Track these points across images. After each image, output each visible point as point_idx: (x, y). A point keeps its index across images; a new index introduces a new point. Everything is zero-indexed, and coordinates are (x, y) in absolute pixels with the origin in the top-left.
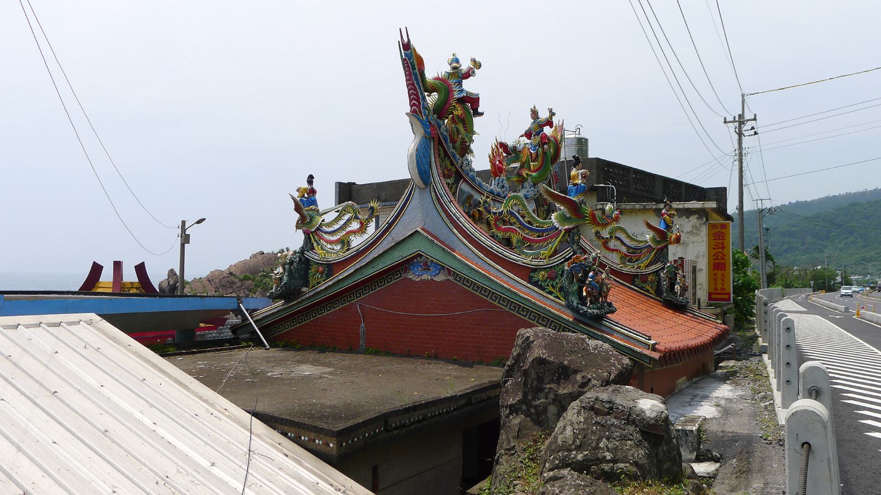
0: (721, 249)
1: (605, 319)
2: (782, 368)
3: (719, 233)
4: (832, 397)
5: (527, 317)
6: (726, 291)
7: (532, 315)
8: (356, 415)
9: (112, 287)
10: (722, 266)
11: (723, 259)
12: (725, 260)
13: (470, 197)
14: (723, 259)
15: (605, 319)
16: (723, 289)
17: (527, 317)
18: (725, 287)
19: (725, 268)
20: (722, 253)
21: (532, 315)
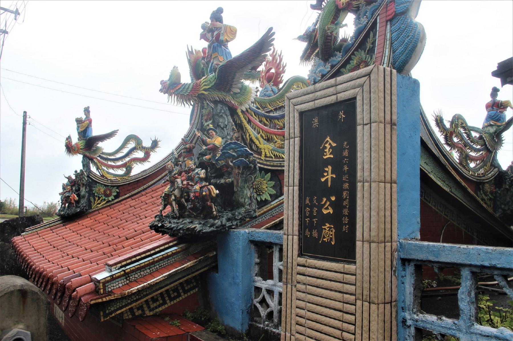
1: (59, 222)
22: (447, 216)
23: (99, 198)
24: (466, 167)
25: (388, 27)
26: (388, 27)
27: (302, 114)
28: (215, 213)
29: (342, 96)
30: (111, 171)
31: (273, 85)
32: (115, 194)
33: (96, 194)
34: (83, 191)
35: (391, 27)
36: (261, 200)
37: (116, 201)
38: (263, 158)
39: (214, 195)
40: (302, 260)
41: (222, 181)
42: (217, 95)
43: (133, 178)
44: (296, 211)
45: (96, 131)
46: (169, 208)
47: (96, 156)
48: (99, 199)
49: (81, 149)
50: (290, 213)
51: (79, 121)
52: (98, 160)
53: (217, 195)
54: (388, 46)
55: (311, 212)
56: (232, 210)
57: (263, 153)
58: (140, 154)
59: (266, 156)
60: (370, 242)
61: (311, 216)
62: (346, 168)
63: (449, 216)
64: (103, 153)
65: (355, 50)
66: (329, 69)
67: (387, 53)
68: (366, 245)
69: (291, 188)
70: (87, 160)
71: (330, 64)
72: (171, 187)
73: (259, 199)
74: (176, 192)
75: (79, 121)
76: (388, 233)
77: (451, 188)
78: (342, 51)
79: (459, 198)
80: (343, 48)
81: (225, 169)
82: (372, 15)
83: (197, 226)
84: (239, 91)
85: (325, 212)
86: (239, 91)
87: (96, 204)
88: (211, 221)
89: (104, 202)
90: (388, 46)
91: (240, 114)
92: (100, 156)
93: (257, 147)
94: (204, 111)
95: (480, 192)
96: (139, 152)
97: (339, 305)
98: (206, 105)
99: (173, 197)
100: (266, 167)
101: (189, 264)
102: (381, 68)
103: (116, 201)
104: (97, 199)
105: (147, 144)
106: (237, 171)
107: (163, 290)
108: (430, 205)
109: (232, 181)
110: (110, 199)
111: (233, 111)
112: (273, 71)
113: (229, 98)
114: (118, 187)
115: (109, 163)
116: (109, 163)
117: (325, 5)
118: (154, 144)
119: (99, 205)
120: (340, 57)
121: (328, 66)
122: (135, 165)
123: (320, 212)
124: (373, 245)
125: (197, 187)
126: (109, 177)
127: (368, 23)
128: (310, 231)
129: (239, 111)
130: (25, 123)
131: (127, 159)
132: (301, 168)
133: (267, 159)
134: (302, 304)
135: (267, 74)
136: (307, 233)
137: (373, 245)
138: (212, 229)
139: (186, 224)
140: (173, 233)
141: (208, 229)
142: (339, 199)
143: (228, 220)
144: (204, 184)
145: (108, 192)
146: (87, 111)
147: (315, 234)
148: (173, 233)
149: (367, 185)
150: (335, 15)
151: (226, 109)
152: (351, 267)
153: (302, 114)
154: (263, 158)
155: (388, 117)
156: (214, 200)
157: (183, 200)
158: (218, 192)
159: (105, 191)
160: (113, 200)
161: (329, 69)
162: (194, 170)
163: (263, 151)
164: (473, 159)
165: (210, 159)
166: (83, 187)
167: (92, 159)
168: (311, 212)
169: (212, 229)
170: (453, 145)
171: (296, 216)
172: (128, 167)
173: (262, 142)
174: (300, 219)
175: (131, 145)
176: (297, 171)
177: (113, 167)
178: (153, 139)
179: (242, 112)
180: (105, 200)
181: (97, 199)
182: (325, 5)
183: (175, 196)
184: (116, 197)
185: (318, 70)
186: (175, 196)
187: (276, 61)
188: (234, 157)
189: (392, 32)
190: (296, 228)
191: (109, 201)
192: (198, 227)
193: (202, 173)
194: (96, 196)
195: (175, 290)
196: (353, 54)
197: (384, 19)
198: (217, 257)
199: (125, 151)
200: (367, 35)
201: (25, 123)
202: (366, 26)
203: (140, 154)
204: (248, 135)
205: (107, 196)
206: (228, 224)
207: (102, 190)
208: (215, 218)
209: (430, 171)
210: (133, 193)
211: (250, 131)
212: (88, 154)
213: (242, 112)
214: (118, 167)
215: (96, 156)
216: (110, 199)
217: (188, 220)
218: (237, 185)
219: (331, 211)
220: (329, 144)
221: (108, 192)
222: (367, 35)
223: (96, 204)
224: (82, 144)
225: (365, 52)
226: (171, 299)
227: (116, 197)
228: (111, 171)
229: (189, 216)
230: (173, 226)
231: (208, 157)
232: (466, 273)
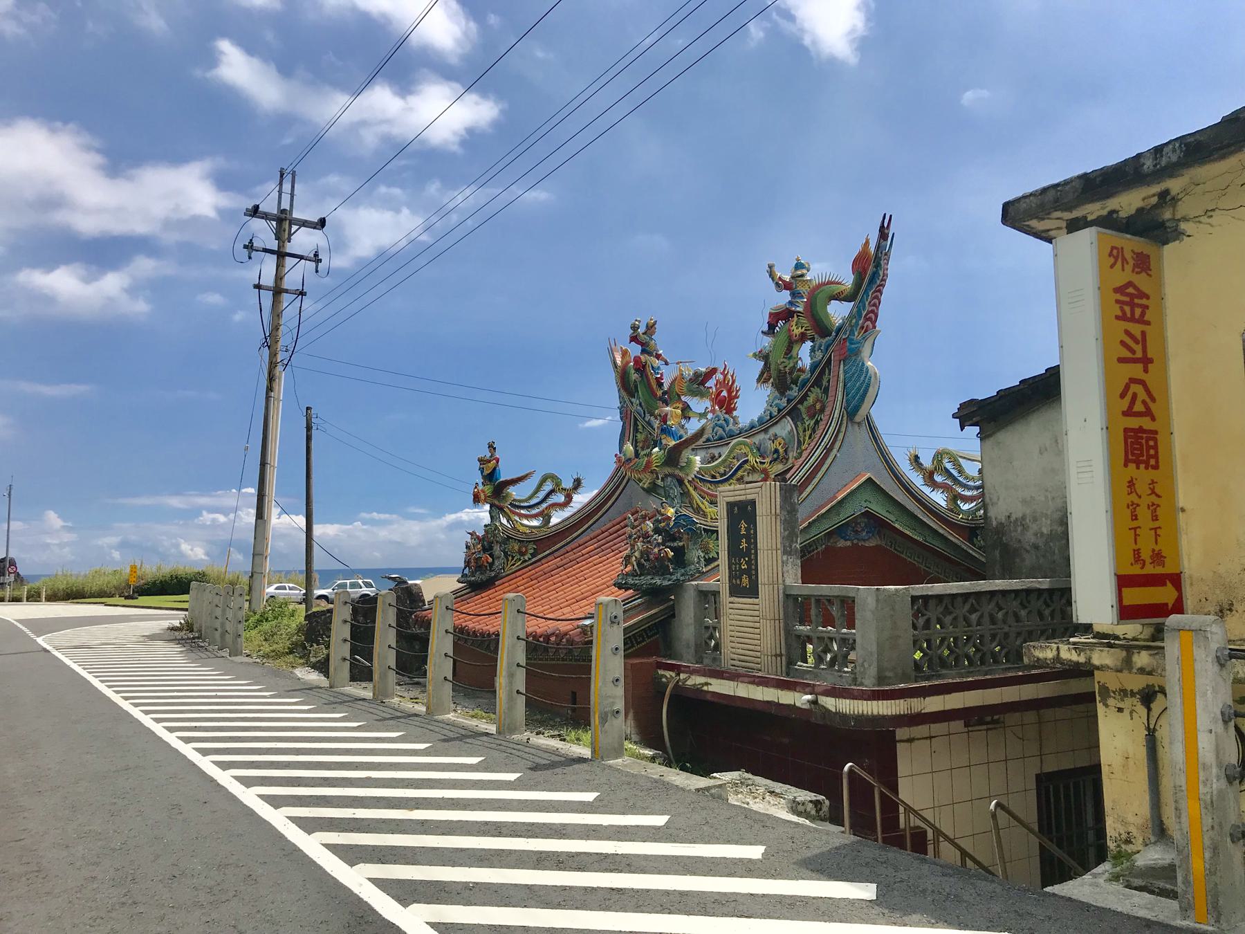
0: (1140, 366)
1: (467, 591)
2: (1053, 819)
3: (1131, 290)
4: (822, 820)
5: (636, 645)
6: (1168, 569)
7: (638, 638)
8: (310, 684)
9: (898, 745)
10: (1149, 448)
11: (1148, 413)
12: (1153, 419)
13: (765, 379)
14: (1148, 413)
15: (467, 591)
16: (1158, 557)
17: (636, 645)
18: (1162, 546)
19: (1156, 457)
20: (1142, 382)
21: (638, 638)
22: (930, 568)
23: (513, 557)
24: (957, 510)
25: (842, 366)
26: (842, 366)
27: (728, 503)
28: (671, 570)
29: (750, 497)
30: (525, 522)
31: (726, 413)
32: (532, 551)
33: (509, 553)
34: (497, 550)
35: (844, 367)
36: (709, 558)
37: (534, 560)
38: (709, 520)
39: (670, 557)
40: (732, 599)
41: (676, 544)
42: (667, 470)
43: (553, 529)
44: (727, 567)
45: (504, 476)
46: (629, 568)
47: (506, 505)
48: (512, 560)
49: (489, 497)
50: (724, 569)
51: (482, 461)
52: (508, 508)
53: (673, 556)
54: (840, 390)
55: (736, 568)
56: (684, 568)
57: (709, 516)
58: (560, 498)
59: (711, 519)
60: (765, 584)
61: (736, 571)
62: (752, 541)
63: (932, 567)
64: (514, 500)
65: (810, 387)
66: (786, 404)
67: (840, 398)
68: (763, 586)
69: (723, 552)
70: (496, 510)
71: (786, 399)
72: (631, 549)
73: (707, 557)
74: (637, 554)
75: (482, 461)
76: (775, 579)
77: (925, 537)
78: (798, 384)
79: (938, 547)
80: (799, 382)
81: (678, 535)
82: (827, 350)
83: (658, 581)
84: (685, 464)
85: (743, 567)
86: (685, 464)
87: (509, 566)
88: (669, 576)
89: (519, 563)
90: (840, 390)
91: (687, 484)
92: (511, 504)
93: (704, 511)
94: (639, 435)
95: (977, 538)
96: (558, 494)
97: (751, 624)
98: (640, 427)
99: (634, 558)
100: (711, 528)
101: (653, 612)
102: (768, 483)
103: (534, 560)
104: (510, 558)
105: (568, 484)
106: (687, 536)
107: (631, 634)
108: (903, 556)
109: (684, 545)
110: (526, 558)
111: (681, 482)
112: (724, 393)
113: (677, 472)
114: (535, 542)
115: (522, 512)
116: (522, 512)
117: (778, 330)
118: (576, 483)
119: (513, 567)
120: (795, 392)
121: (785, 400)
122: (554, 512)
123: (740, 567)
124: (766, 586)
125: (656, 550)
126: (522, 529)
127: (823, 358)
128: (736, 580)
129: (686, 482)
130: (309, 428)
131: (544, 505)
132: (728, 539)
133: (713, 521)
134: (732, 628)
135: (719, 398)
136: (734, 581)
137: (766, 586)
138: (670, 582)
139: (646, 580)
140: (634, 587)
141: (666, 583)
142: (750, 559)
143: (682, 575)
144: (661, 547)
145: (524, 549)
146: (491, 447)
147: (738, 582)
148: (634, 587)
149: (762, 551)
150: (789, 346)
151: (675, 481)
152: (756, 601)
153: (728, 503)
154: (709, 520)
155: (773, 512)
156: (669, 560)
157: (642, 560)
158: (673, 553)
159: (520, 548)
160: (530, 559)
161: (786, 404)
162: (653, 536)
163: (709, 514)
164: (966, 499)
165: (664, 526)
166: (497, 545)
167: (501, 509)
168: (736, 568)
169: (670, 582)
170: (934, 485)
171: (727, 571)
172: (547, 518)
173: (707, 507)
174: (730, 573)
175: (548, 487)
176: (726, 541)
177: (527, 517)
178: (575, 477)
179: (689, 481)
180: (520, 560)
181: (510, 558)
182: (778, 330)
183: (636, 557)
184: (533, 555)
185: (774, 403)
186: (636, 557)
187: (728, 382)
188: (685, 526)
189: (845, 373)
190: (727, 579)
191: (525, 561)
192: (659, 582)
193: (660, 539)
194: (509, 555)
195: (641, 636)
196: (809, 390)
197: (837, 358)
198: (674, 607)
199: (541, 495)
200: (822, 373)
201: (309, 428)
202: (821, 361)
203: (560, 498)
204: (695, 501)
205: (523, 554)
206: (682, 578)
207: (516, 548)
208: (672, 574)
209: (894, 519)
210: (554, 549)
211: (696, 498)
212: (497, 503)
213: (689, 481)
214: (535, 516)
215: (506, 505)
216: (526, 558)
217: (649, 577)
218: (688, 548)
219: (746, 567)
220: (743, 525)
221: (524, 549)
222: (822, 373)
223: (509, 566)
224: (488, 489)
225: (821, 389)
226: (638, 643)
227: (533, 555)
228: (525, 522)
229: (648, 574)
230: (636, 582)
231: (663, 524)
232: (813, 600)
